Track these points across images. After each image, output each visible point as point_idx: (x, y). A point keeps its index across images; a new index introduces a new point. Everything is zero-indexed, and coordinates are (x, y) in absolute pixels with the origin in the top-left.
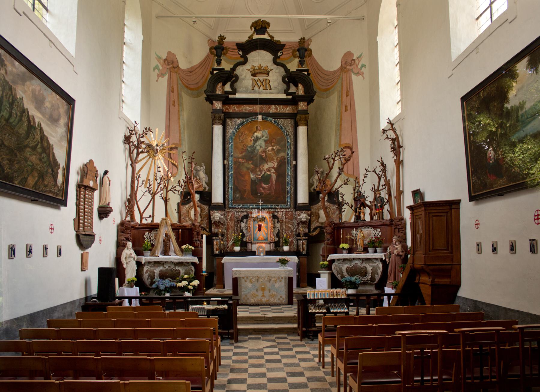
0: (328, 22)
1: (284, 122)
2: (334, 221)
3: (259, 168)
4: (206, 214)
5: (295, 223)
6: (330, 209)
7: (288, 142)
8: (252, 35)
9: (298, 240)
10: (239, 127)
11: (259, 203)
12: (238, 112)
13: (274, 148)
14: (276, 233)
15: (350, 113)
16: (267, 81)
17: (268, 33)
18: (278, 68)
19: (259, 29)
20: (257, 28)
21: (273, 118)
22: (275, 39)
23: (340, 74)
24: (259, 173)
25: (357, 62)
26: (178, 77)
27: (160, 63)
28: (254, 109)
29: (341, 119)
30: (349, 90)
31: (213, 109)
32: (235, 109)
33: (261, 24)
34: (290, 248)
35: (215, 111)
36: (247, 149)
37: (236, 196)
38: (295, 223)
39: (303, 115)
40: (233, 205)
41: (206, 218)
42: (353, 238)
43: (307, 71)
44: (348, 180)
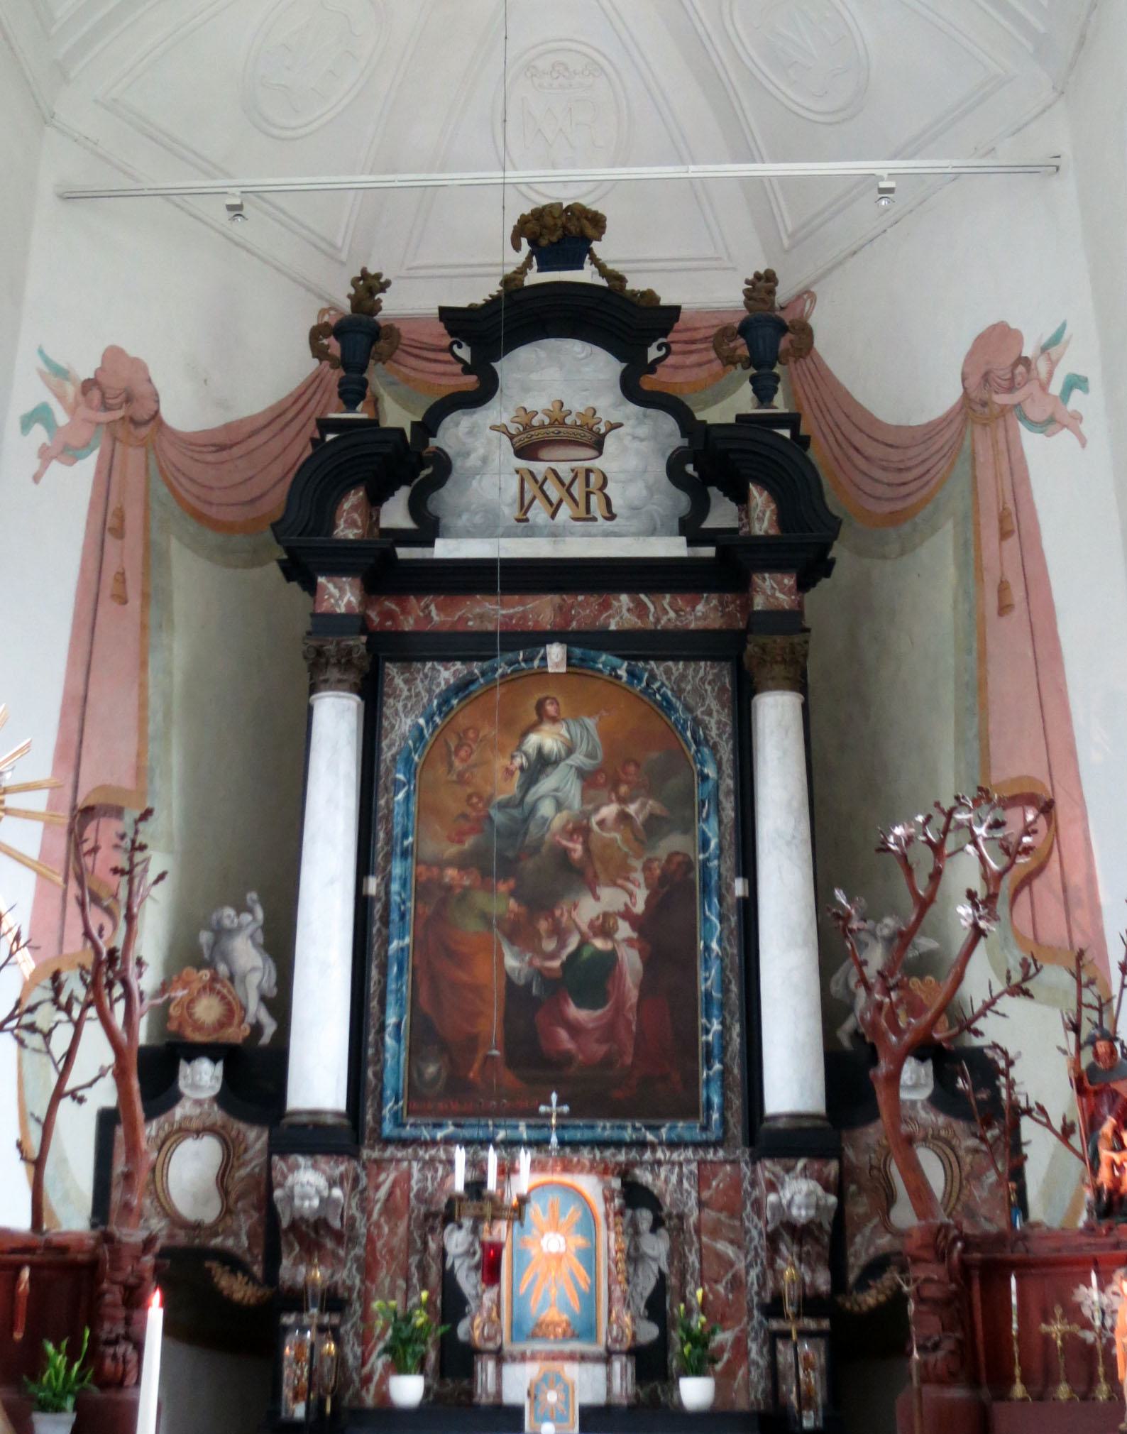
0: (882, 191)
1: (683, 677)
2: (958, 1226)
3: (552, 915)
4: (250, 1175)
5: (755, 1233)
6: (953, 1149)
7: (705, 778)
8: (522, 271)
9: (773, 1338)
10: (445, 701)
11: (548, 1116)
12: (446, 628)
13: (632, 809)
14: (647, 1293)
15: (1025, 617)
16: (593, 477)
17: (595, 261)
18: (645, 416)
19: (551, 243)
20: (544, 242)
21: (624, 658)
22: (629, 287)
23: (961, 434)
24: (549, 945)
25: (1042, 367)
26: (153, 465)
27: (61, 398)
28: (524, 617)
29: (982, 657)
30: (1010, 506)
31: (314, 615)
32: (428, 617)
33: (559, 223)
34: (719, 1389)
35: (326, 623)
36: (489, 818)
37: (421, 1074)
38: (756, 1231)
39: (779, 639)
40: (403, 1125)
41: (253, 1198)
42: (1089, 1336)
43: (792, 421)
44: (1029, 969)
